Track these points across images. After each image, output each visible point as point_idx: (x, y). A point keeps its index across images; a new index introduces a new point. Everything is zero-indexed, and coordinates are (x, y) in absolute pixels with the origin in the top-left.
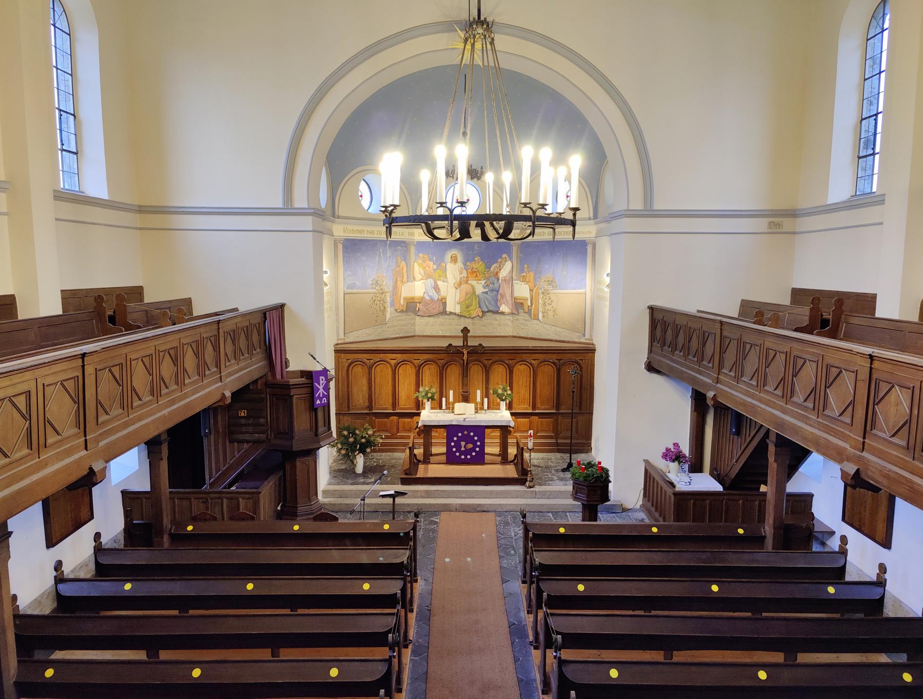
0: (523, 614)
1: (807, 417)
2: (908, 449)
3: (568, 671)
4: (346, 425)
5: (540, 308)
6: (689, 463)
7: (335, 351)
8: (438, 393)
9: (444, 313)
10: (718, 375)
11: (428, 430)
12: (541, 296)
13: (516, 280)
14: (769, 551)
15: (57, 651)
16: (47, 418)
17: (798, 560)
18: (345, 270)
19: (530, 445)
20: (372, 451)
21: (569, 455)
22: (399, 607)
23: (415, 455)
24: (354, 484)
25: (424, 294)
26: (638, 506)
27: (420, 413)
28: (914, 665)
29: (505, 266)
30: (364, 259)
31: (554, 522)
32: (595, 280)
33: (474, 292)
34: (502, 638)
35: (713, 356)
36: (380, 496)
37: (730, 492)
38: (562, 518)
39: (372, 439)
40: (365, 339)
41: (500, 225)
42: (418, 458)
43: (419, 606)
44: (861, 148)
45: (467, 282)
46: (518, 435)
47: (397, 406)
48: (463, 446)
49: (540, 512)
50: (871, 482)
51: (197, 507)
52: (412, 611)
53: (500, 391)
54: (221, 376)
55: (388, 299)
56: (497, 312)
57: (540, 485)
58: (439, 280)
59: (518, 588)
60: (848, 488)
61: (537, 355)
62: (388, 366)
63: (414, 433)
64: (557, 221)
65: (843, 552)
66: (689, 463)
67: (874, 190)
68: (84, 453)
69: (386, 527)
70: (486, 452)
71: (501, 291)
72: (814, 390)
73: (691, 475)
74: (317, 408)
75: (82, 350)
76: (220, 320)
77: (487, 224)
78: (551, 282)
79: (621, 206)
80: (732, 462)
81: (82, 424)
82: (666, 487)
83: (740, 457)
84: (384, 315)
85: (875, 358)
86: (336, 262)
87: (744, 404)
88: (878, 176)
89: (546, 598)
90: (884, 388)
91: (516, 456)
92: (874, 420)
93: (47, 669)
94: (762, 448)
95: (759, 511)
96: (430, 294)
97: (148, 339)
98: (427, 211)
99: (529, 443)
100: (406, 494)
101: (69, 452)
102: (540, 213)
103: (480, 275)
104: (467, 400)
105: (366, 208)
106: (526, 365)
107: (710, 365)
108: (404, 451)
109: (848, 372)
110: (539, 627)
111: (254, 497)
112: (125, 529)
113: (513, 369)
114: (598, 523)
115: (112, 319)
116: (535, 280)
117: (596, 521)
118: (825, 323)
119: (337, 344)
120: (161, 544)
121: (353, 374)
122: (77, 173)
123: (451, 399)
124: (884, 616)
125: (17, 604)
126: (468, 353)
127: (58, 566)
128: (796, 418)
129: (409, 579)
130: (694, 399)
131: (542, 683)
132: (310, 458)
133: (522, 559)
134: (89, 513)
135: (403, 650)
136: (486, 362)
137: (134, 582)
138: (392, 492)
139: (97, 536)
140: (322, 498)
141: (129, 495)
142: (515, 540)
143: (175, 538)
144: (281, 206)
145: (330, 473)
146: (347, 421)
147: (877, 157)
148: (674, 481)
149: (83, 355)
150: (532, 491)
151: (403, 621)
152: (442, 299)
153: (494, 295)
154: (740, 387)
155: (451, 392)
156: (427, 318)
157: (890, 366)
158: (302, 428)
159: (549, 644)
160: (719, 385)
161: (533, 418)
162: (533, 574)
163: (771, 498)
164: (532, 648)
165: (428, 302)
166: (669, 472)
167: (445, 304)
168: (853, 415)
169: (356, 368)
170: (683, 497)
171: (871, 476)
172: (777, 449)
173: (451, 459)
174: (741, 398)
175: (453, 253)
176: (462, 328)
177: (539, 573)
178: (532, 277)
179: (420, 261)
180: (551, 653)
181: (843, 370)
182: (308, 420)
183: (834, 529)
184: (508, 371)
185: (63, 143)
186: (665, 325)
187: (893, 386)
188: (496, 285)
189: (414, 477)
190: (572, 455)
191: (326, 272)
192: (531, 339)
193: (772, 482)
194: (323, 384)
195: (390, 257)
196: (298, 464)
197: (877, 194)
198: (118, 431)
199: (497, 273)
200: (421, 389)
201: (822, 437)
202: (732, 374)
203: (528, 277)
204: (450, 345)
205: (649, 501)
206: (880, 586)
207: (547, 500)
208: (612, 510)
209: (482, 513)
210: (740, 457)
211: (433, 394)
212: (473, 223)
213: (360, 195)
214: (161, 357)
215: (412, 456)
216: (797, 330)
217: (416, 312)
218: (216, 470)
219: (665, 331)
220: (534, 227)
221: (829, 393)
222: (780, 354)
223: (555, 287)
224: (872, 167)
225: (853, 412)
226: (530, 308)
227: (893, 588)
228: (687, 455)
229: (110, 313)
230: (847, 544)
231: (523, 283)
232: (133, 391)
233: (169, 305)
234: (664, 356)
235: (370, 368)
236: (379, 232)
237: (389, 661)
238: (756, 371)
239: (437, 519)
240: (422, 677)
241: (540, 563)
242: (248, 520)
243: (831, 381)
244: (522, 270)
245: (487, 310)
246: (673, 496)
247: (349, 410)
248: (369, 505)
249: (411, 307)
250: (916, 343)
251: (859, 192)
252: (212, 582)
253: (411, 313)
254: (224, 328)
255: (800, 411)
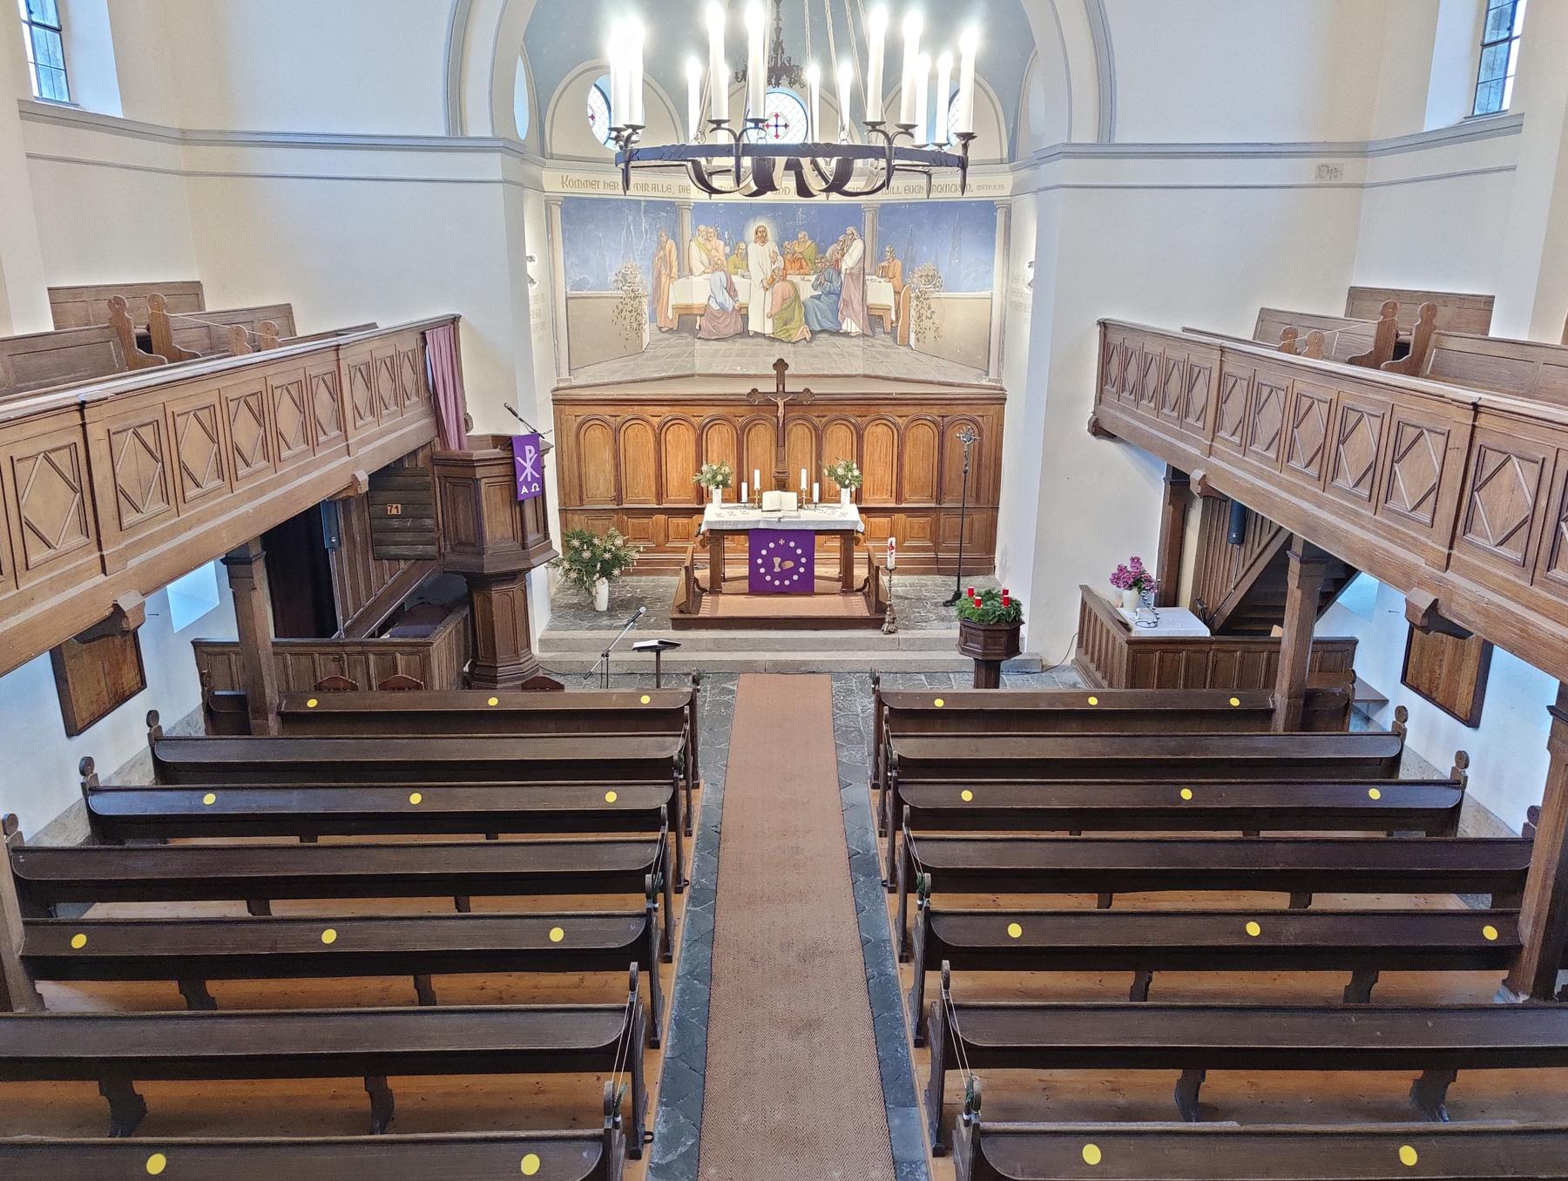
0: (873, 837)
1: (1356, 512)
2: (1524, 566)
3: (942, 929)
4: (577, 530)
5: (911, 326)
6: (1156, 591)
7: (553, 400)
8: (735, 474)
9: (744, 333)
10: (1212, 441)
11: (717, 537)
12: (914, 303)
13: (869, 275)
14: (1278, 733)
15: (98, 904)
16: (25, 517)
17: (1323, 746)
18: (567, 254)
19: (891, 563)
20: (622, 573)
21: (956, 579)
22: (665, 830)
23: (696, 581)
24: (594, 629)
25: (709, 299)
26: (1068, 662)
27: (704, 509)
28: (1502, 914)
29: (852, 248)
30: (601, 235)
31: (928, 689)
32: (1008, 275)
33: (797, 296)
34: (839, 877)
35: (1204, 409)
36: (635, 649)
37: (1221, 638)
38: (941, 683)
39: (622, 553)
40: (607, 380)
41: (830, 165)
42: (702, 586)
43: (703, 826)
44: (1489, 27)
45: (784, 279)
46: (870, 544)
47: (665, 496)
48: (777, 565)
49: (906, 673)
50: (1455, 621)
51: (326, 668)
52: (689, 834)
53: (840, 471)
54: (348, 445)
55: (645, 308)
56: (837, 333)
57: (907, 628)
58: (734, 274)
59: (867, 798)
60: (1416, 630)
61: (904, 408)
62: (648, 428)
63: (695, 543)
64: (939, 159)
65: (1399, 733)
66: (1156, 591)
67: (1506, 106)
68: (101, 578)
69: (645, 700)
70: (816, 574)
71: (843, 295)
72: (1372, 467)
73: (1158, 610)
74: (522, 501)
75: (77, 396)
76: (339, 345)
77: (805, 162)
78: (931, 279)
79: (1056, 137)
80: (1229, 590)
81: (92, 527)
82: (1116, 631)
83: (1240, 581)
84: (640, 337)
85: (1482, 409)
86: (551, 242)
87: (1253, 491)
88: (1515, 80)
89: (907, 814)
90: (1493, 460)
91: (867, 581)
92: (1470, 518)
93: (77, 934)
94: (1278, 566)
95: (1267, 671)
96: (719, 300)
97: (205, 377)
98: (696, 139)
99: (889, 559)
100: (678, 645)
101: (72, 578)
102: (901, 142)
103: (807, 265)
104: (784, 487)
105: (602, 142)
106: (887, 425)
107: (1200, 424)
108: (677, 573)
109: (1433, 435)
110: (897, 857)
111: (421, 650)
112: (203, 703)
113: (863, 434)
114: (1000, 690)
115: (145, 343)
116: (904, 275)
117: (997, 686)
118: (1401, 349)
119: (558, 389)
120: (264, 729)
121: (587, 440)
122: (63, 68)
123: (757, 486)
124: (1458, 836)
125: (19, 829)
126: (785, 405)
127: (87, 766)
128: (1336, 514)
129: (683, 783)
130: (1171, 483)
131: (900, 945)
132: (516, 586)
133: (872, 750)
134: (138, 678)
135: (674, 897)
136: (816, 421)
137: (219, 792)
138: (655, 643)
139: (153, 717)
140: (540, 651)
141: (210, 649)
142: (863, 718)
143: (287, 718)
144: (443, 134)
145: (552, 610)
146: (578, 523)
147: (1516, 44)
148: (1129, 621)
149: (82, 406)
150: (893, 639)
151: (672, 850)
152: (741, 308)
153: (832, 301)
154: (1248, 462)
155: (757, 473)
156: (715, 342)
157: (1508, 424)
158: (498, 535)
159: (911, 885)
160: (1212, 459)
161: (896, 516)
162: (889, 774)
163: (1287, 648)
164: (886, 890)
165: (716, 314)
166: (1122, 606)
167: (745, 318)
168: (1435, 508)
169: (591, 432)
170: (1141, 646)
171: (1456, 612)
172: (1304, 566)
173: (757, 586)
174: (1247, 481)
175: (758, 225)
176: (775, 361)
177: (898, 773)
178: (899, 269)
179: (701, 240)
180: (914, 900)
181: (1424, 431)
182: (509, 521)
183: (1388, 698)
184: (855, 435)
185: (32, 9)
186: (1127, 354)
187: (1509, 458)
188: (835, 283)
189: (694, 616)
190: (962, 579)
191: (532, 259)
192: (896, 379)
193: (1290, 622)
194: (531, 460)
195: (646, 230)
196: (495, 596)
197: (1508, 114)
198: (162, 541)
199: (837, 261)
200: (705, 468)
201: (1380, 547)
202: (1236, 439)
203: (892, 267)
204: (754, 391)
205: (1086, 653)
206: (1455, 788)
207: (917, 652)
208: (1024, 669)
209: (809, 675)
210: (1240, 581)
211: (726, 477)
212: (781, 161)
213: (590, 115)
214: (232, 411)
215: (691, 581)
216: (1352, 361)
217: (695, 333)
218: (354, 604)
219: (1125, 366)
220: (891, 170)
221: (1397, 471)
222: (1371, 418)
223: (939, 287)
224: (1504, 63)
225: (1436, 504)
226: (894, 325)
227: (1475, 789)
228: (1154, 577)
229: (142, 330)
230: (1405, 721)
231: (882, 280)
232: (183, 470)
233: (249, 317)
234: (1123, 410)
235: (617, 431)
236: (613, 185)
237: (648, 916)
238: (1277, 434)
239: (733, 685)
240: (706, 938)
241: (899, 756)
242: (410, 689)
243: (1403, 449)
244: (881, 258)
245: (818, 329)
246: (1126, 647)
247: (582, 504)
248: (617, 663)
249: (686, 322)
250: (1555, 383)
251: (1480, 109)
252: (350, 791)
253: (687, 335)
254: (349, 358)
255: (1346, 503)
